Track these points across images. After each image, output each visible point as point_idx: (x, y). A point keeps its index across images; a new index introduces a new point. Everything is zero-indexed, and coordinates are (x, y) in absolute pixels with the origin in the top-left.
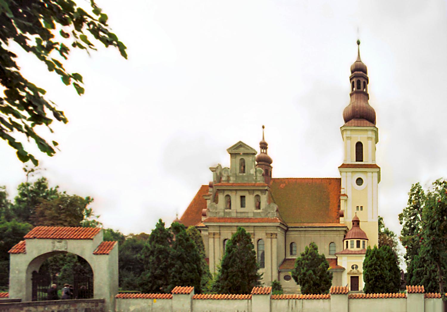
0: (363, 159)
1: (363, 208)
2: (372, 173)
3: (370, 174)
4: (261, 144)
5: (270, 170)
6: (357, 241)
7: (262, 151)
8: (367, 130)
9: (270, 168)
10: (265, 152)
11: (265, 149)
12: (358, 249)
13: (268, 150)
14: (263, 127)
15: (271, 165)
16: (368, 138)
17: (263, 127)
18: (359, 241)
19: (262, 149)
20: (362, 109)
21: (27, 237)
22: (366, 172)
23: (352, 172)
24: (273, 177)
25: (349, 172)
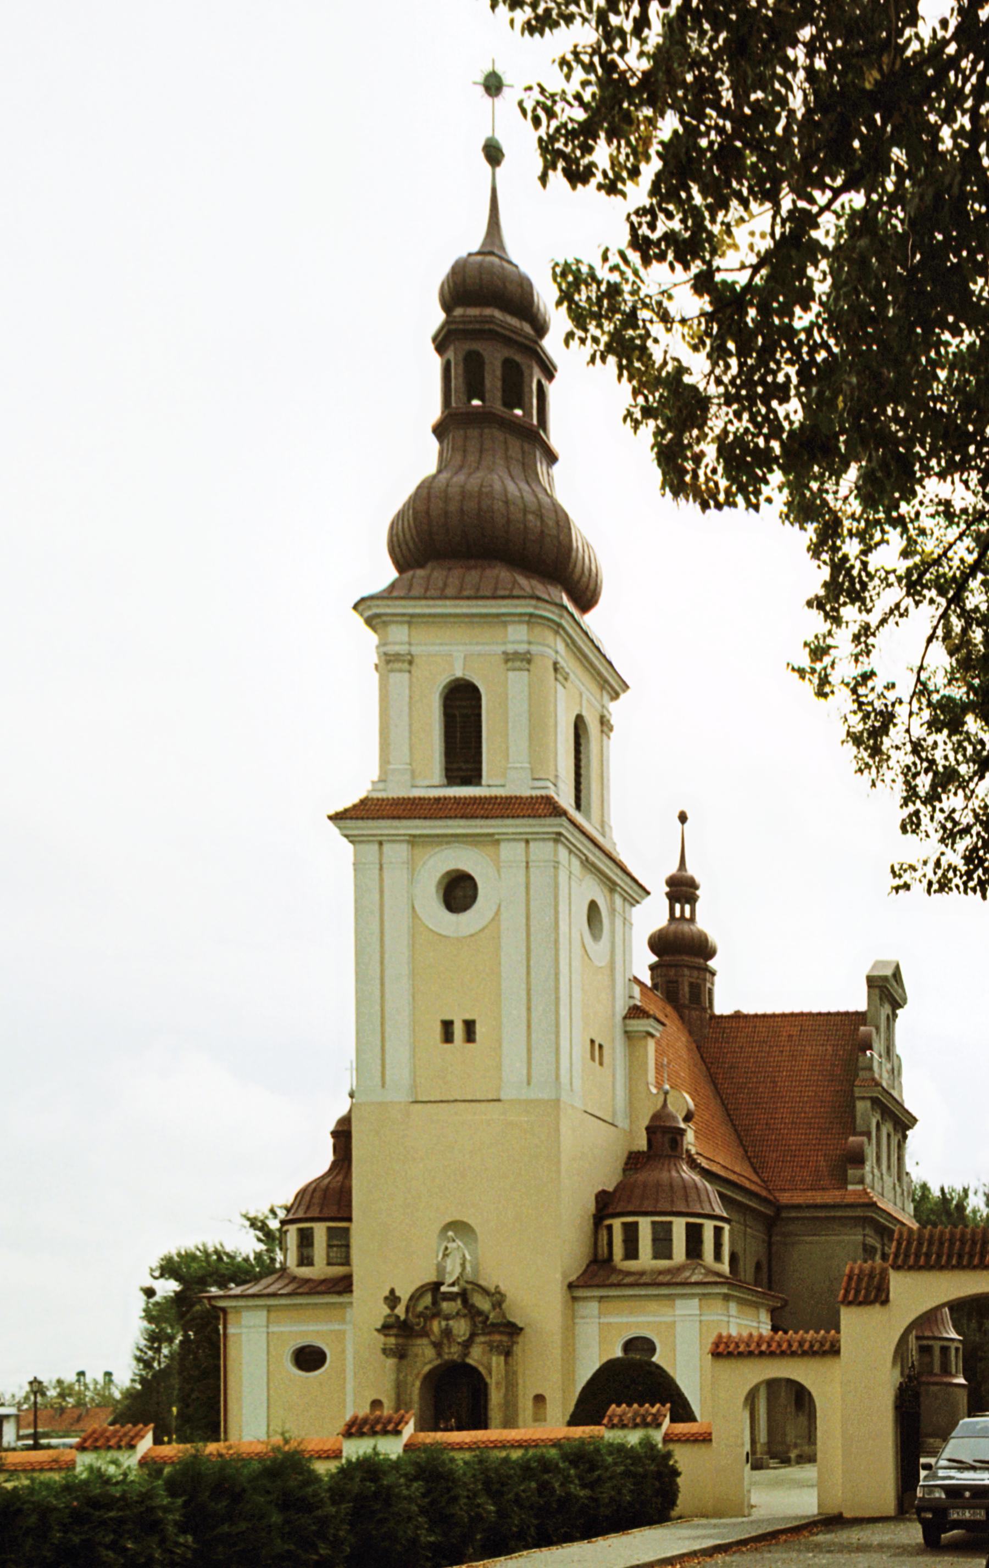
0: (479, 770)
1: (479, 1029)
2: (527, 842)
3: (511, 852)
4: (672, 882)
5: (708, 985)
6: (625, 1225)
7: (678, 914)
8: (498, 615)
9: (708, 975)
10: (687, 915)
11: (688, 902)
12: (663, 1264)
13: (698, 905)
14: (683, 818)
15: (711, 963)
16: (509, 658)
17: (683, 818)
18: (700, 1226)
19: (678, 901)
20: (471, 505)
21: (615, 1282)
22: (494, 840)
23: (413, 841)
24: (723, 1005)
25: (394, 839)
